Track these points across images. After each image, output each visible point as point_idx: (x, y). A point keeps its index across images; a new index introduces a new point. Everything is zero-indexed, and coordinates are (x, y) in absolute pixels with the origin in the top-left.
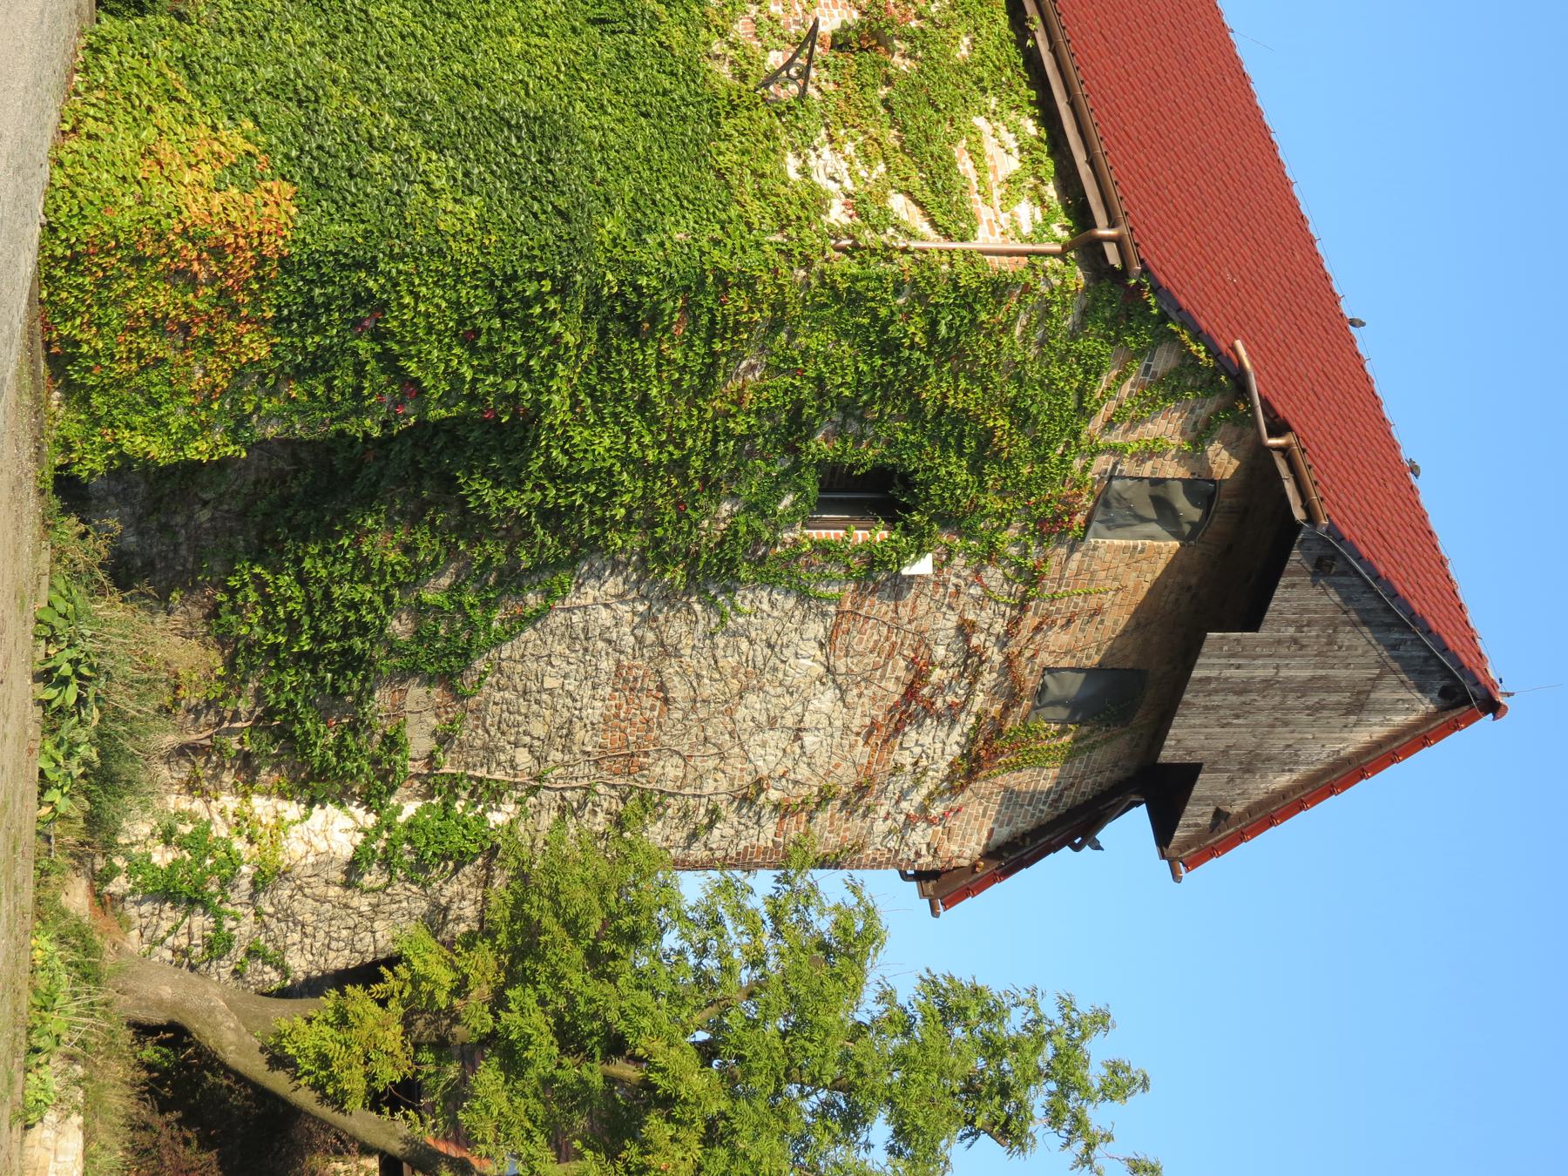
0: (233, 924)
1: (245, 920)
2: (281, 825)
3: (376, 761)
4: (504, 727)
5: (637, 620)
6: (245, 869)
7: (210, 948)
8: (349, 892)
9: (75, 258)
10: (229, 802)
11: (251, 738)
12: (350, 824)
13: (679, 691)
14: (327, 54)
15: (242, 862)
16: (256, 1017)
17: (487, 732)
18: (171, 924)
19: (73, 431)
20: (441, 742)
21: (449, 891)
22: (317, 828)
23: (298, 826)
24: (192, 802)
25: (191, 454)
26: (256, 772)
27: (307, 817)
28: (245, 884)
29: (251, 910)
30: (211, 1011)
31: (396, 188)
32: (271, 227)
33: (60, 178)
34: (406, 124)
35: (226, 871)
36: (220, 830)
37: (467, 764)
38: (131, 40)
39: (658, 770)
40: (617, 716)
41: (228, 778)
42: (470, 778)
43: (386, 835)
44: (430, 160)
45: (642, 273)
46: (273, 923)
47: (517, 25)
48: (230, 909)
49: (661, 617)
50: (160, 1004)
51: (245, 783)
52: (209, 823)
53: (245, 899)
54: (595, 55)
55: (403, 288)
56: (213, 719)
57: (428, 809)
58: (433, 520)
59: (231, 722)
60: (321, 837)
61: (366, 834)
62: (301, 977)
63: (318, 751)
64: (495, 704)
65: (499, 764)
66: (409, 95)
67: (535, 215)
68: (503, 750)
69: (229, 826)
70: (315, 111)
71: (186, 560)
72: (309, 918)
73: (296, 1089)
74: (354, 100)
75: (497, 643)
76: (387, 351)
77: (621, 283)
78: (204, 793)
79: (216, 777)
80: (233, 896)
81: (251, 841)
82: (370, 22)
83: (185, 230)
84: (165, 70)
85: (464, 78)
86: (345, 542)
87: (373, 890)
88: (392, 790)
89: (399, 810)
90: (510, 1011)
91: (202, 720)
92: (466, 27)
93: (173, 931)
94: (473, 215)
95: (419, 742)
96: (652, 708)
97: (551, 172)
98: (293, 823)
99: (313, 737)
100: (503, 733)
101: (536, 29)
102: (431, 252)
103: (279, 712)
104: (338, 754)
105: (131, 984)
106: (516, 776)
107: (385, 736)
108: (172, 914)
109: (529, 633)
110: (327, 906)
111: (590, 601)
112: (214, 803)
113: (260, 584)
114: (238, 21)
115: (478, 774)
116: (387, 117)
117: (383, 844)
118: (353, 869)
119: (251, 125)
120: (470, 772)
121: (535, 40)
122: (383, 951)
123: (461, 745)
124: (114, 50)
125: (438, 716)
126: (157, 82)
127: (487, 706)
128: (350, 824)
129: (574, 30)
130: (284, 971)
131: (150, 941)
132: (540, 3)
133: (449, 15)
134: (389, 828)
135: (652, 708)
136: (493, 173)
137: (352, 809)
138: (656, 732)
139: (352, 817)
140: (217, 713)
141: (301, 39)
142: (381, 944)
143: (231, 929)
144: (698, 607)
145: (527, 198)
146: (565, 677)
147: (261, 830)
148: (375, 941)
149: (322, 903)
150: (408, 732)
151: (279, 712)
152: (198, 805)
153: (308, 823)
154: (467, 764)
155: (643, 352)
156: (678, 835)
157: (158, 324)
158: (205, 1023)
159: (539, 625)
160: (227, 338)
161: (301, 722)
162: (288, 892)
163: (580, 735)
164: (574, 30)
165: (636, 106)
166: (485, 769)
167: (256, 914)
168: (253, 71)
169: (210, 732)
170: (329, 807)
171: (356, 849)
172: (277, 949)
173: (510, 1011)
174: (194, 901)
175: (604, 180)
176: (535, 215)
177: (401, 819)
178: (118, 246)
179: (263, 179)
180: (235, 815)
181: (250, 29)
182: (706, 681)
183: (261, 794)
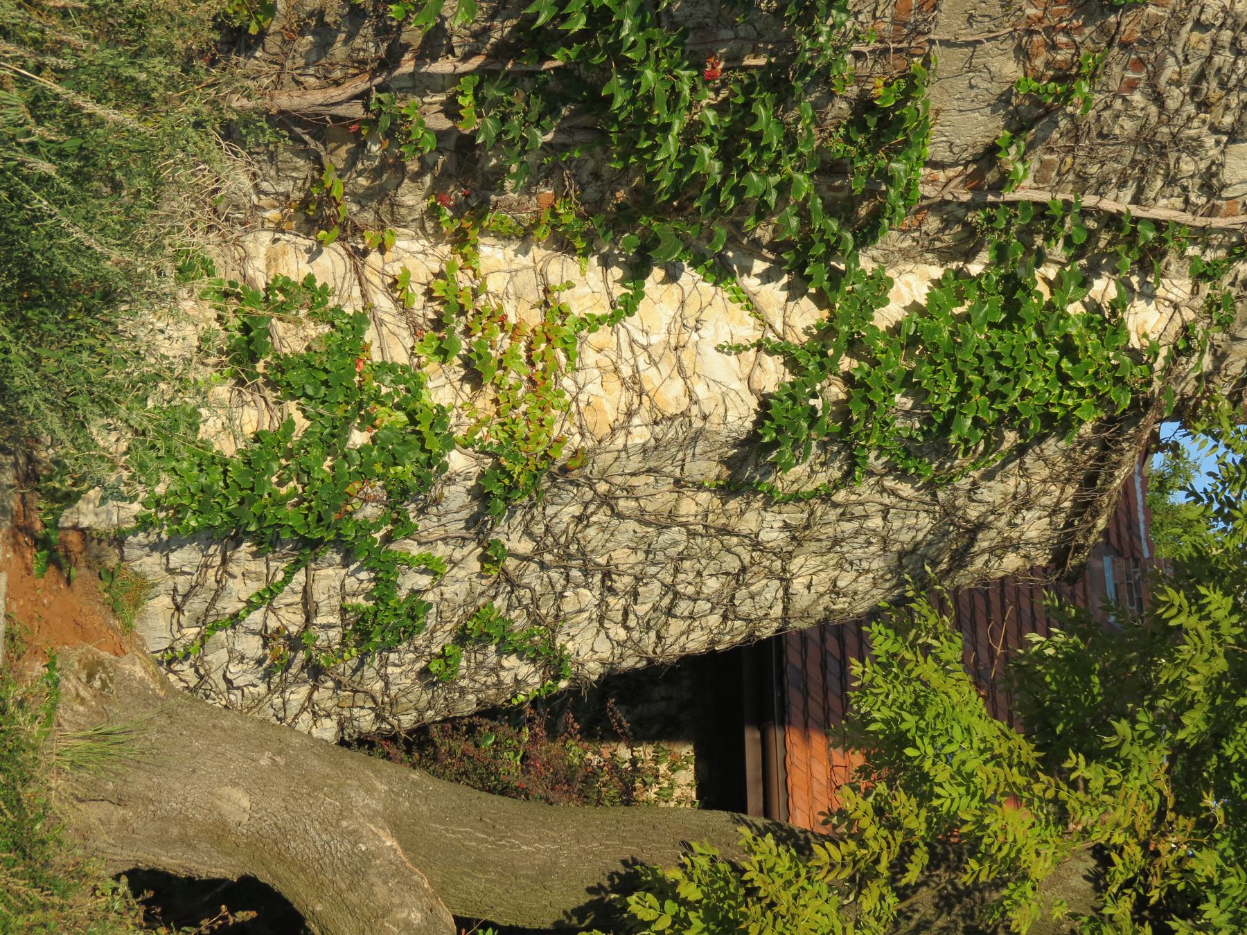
0: (424, 581)
1: (459, 573)
3: (830, 169)
4: (1211, 88)
6: (457, 461)
7: (364, 636)
8: (733, 505)
11: (480, 101)
12: (747, 330)
16: (481, 864)
17: (1158, 99)
18: (254, 587)
20: (1019, 125)
21: (992, 493)
23: (602, 336)
24: (314, 254)
26: (494, 181)
27: (629, 306)
28: (457, 496)
29: (472, 552)
30: (359, 869)
35: (406, 471)
37: (1082, 178)
41: (412, 197)
42: (1085, 213)
46: (532, 576)
48: (415, 550)
50: (219, 833)
51: (458, 210)
52: (359, 322)
53: (456, 528)
56: (368, 46)
57: (957, 284)
59: (420, 58)
60: (665, 368)
61: (792, 363)
62: (594, 670)
63: (672, 144)
64: (1199, 26)
65: (1171, 180)
68: (1194, 148)
69: (416, 331)
72: (623, 557)
78: (348, 230)
79: (380, 195)
80: (427, 525)
81: (474, 377)
87: (797, 498)
88: (867, 234)
89: (879, 287)
91: (339, 50)
93: (266, 597)
98: (590, 323)
99: (659, 113)
100: (1204, 106)
103: (567, 40)
104: (727, 154)
105: (139, 782)
106: (1212, 212)
107: (864, 105)
108: (258, 566)
110: (676, 533)
112: (374, 258)
115: (1108, 205)
117: (837, 391)
120: (1089, 200)
122: (805, 614)
123: (1075, 133)
125: (1023, 54)
127: (1173, 32)
128: (747, 330)
130: (553, 663)
131: (198, 620)
134: (854, 346)
137: (751, 283)
139: (751, 305)
140: (383, 31)
142: (802, 599)
143: (415, 592)
147: (503, 341)
148: (787, 596)
149: (662, 528)
150: (932, 95)
151: (567, 40)
153: (632, 322)
154: (1082, 178)
161: (631, 74)
162: (576, 510)
166: (1128, 193)
167: (484, 559)
169: (361, 84)
170: (689, 276)
171: (765, 403)
172: (537, 620)
177: (887, 316)
180: (429, 294)
183: (504, 237)
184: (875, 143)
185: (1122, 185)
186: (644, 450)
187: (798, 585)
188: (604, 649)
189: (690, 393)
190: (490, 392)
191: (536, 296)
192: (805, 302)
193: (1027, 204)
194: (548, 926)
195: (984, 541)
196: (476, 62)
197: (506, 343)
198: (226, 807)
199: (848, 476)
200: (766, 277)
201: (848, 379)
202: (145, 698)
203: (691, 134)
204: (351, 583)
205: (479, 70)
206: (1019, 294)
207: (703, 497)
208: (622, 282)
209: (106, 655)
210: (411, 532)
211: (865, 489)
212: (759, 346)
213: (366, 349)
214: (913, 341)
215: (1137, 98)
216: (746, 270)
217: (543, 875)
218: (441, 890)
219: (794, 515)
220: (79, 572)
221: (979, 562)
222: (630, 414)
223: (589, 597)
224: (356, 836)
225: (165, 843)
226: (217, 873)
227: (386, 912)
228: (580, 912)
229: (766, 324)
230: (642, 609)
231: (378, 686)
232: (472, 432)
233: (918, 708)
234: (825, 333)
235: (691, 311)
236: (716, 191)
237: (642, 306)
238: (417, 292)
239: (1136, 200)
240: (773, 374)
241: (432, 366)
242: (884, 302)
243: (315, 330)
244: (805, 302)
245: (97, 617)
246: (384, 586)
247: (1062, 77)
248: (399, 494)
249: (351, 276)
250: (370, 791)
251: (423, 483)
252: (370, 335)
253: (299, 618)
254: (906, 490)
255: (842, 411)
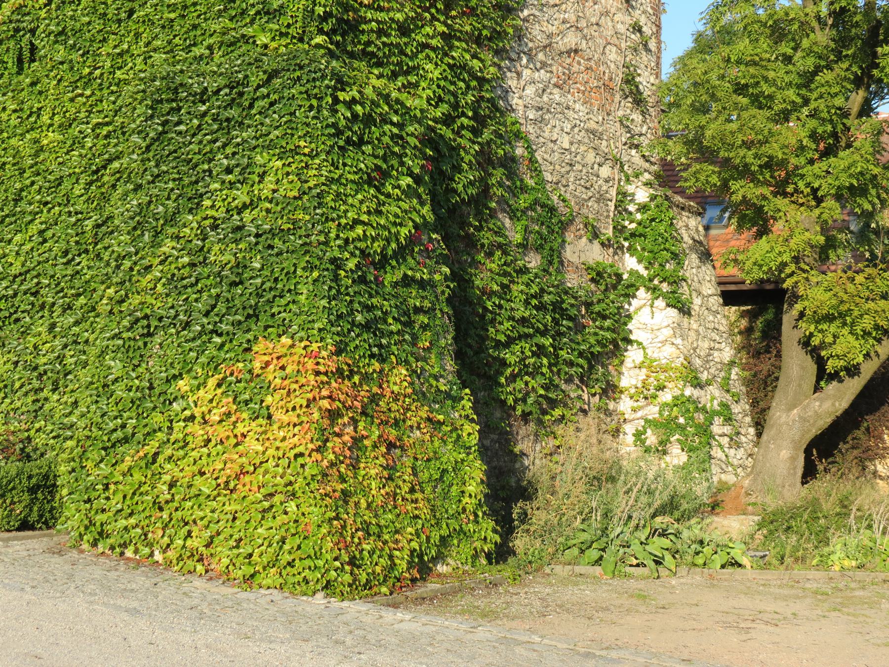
2: (648, 364)
5: (531, 66)
8: (693, 313)
9: (352, 562)
10: (625, 405)
13: (571, 40)
14: (64, 311)
15: (682, 395)
16: (800, 385)
19: (466, 550)
22: (650, 336)
23: (649, 351)
24: (625, 434)
25: (474, 440)
27: (639, 343)
28: (696, 393)
30: (803, 419)
31: (253, 239)
32: (310, 364)
33: (271, 577)
34: (170, 231)
35: (691, 407)
36: (652, 412)
38: (89, 501)
39: (612, 66)
40: (584, 92)
43: (656, 282)
44: (213, 207)
45: (313, 11)
46: (712, 371)
47: (28, 136)
49: (530, 45)
50: (793, 459)
52: (646, 421)
54: (62, 63)
55: (352, 235)
58: (476, 228)
60: (658, 333)
61: (657, 298)
66: (135, 229)
67: (272, 104)
69: (648, 405)
70: (160, 319)
71: (492, 440)
73: (878, 355)
74: (145, 281)
75: (542, 182)
76: (395, 255)
77: (321, 31)
80: (703, 401)
81: (661, 388)
82: (28, 271)
83: (318, 450)
84: (124, 467)
85: (90, 183)
86: (489, 305)
89: (632, 272)
90: (820, 186)
92: (33, 183)
93: (720, 446)
94: (279, 163)
95: (595, 254)
96: (579, 63)
97: (217, 92)
99: (600, 338)
101: (32, 119)
102: (320, 205)
104: (604, 317)
105: (779, 481)
106: (614, 179)
109: (538, 156)
111: (520, 102)
112: (626, 416)
113: (513, 378)
114: (26, 394)
115: (613, 208)
116: (164, 249)
118: (685, 310)
119: (181, 383)
120: (611, 214)
121: (45, 119)
124: (100, 518)
126: (138, 476)
128: (647, 310)
129: (33, 84)
130: (732, 363)
132: (4, 116)
133: (16, 201)
134: (651, 280)
135: (579, 63)
136: (225, 146)
137: (632, 309)
138: (592, 63)
139: (639, 309)
141: (45, 336)
144: (526, 13)
145: (253, 112)
146: (563, 130)
147: (651, 380)
149: (699, 334)
150: (591, 263)
152: (629, 429)
153: (644, 344)
155: (370, 21)
156: (645, 58)
157: (390, 474)
158: (813, 425)
159: (534, 147)
160: (394, 407)
163: (592, 125)
164: (33, 84)
165: (119, 21)
166: (609, 203)
168: (116, 380)
171: (668, 305)
173: (820, 186)
174: (705, 431)
175: (210, 48)
176: (272, 104)
177: (645, 273)
178: (337, 518)
179: (250, 372)
181: (36, 384)
182: (566, 16)
184: (602, 277)
185: (607, 205)
186: (683, 340)
187: (710, 292)
188: (728, 349)
189: (666, 327)
190: (666, 384)
191: (637, 370)
192: (637, 293)
193: (614, 233)
194: (816, 366)
195: (697, 238)
196: (584, 388)
197: (652, 379)
198: (786, 457)
199: (685, 280)
200: (630, 304)
201: (661, 282)
202: (755, 480)
203: (601, 328)
204: (717, 423)
205: (587, 387)
206: (637, 233)
207: (692, 322)
208: (632, 345)
209: (743, 491)
210: (705, 406)
211: (687, 275)
212: (652, 307)
213: (655, 419)
214: (650, 263)
215: (590, 204)
216: (628, 310)
217: (803, 368)
218: (807, 397)
219: (694, 294)
220: (719, 498)
221: (702, 238)
222: (673, 344)
223: (716, 354)
224: (794, 421)
225: (795, 473)
226: (803, 460)
227: (816, 412)
228: (812, 357)
229: (645, 305)
230: (718, 338)
231: (740, 415)
232: (679, 389)
233: (761, 266)
234: (648, 289)
235: (641, 326)
236: (615, 321)
237: (640, 340)
238: (636, 404)
239: (611, 201)
240: (660, 303)
241: (659, 400)
242: (637, 272)
243: (649, 432)
244: (637, 293)
245: (733, 493)
246: (719, 414)
247: (586, 226)
248: (697, 409)
249: (632, 423)
250: (780, 417)
251: (694, 402)
252: (650, 417)
253: (726, 437)
254: (687, 263)
255: (670, 284)
